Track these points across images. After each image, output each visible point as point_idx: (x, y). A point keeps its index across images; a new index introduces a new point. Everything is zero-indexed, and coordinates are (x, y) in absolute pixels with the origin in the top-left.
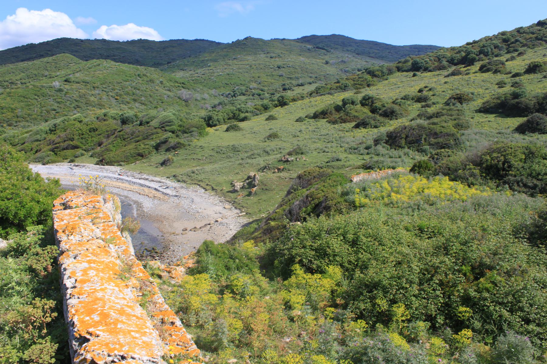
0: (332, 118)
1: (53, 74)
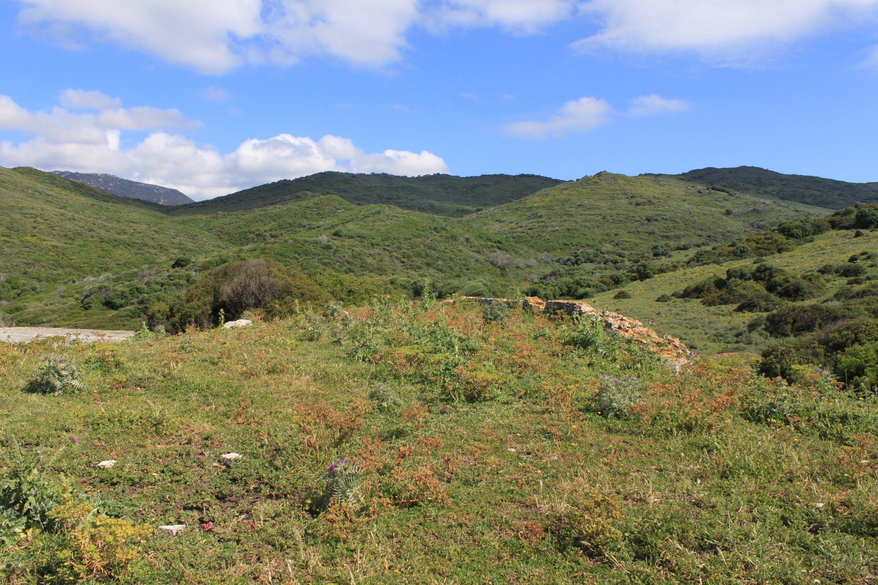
0: (709, 297)
1: (314, 223)
